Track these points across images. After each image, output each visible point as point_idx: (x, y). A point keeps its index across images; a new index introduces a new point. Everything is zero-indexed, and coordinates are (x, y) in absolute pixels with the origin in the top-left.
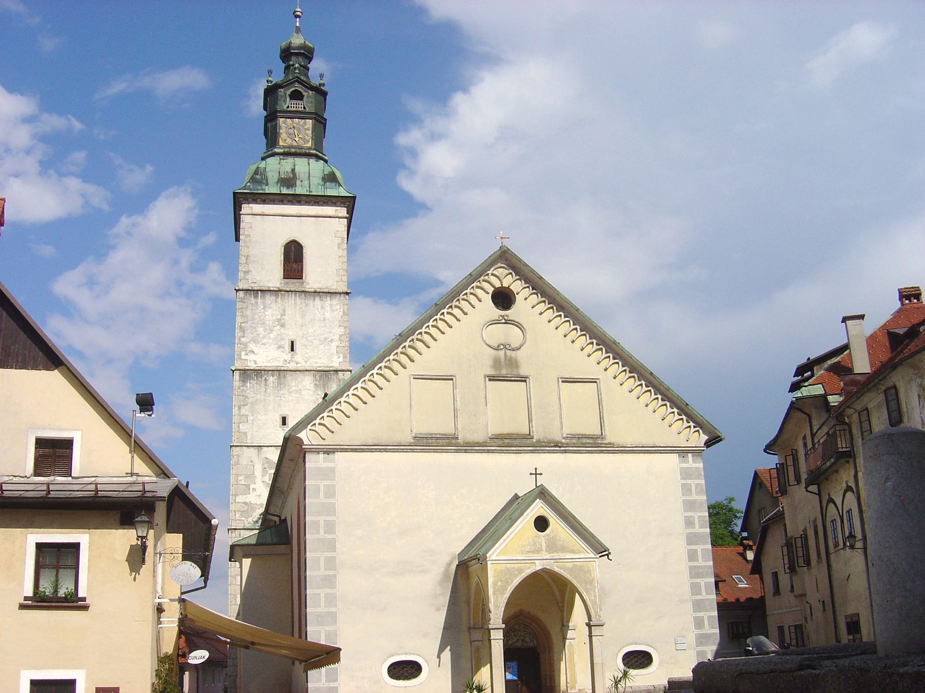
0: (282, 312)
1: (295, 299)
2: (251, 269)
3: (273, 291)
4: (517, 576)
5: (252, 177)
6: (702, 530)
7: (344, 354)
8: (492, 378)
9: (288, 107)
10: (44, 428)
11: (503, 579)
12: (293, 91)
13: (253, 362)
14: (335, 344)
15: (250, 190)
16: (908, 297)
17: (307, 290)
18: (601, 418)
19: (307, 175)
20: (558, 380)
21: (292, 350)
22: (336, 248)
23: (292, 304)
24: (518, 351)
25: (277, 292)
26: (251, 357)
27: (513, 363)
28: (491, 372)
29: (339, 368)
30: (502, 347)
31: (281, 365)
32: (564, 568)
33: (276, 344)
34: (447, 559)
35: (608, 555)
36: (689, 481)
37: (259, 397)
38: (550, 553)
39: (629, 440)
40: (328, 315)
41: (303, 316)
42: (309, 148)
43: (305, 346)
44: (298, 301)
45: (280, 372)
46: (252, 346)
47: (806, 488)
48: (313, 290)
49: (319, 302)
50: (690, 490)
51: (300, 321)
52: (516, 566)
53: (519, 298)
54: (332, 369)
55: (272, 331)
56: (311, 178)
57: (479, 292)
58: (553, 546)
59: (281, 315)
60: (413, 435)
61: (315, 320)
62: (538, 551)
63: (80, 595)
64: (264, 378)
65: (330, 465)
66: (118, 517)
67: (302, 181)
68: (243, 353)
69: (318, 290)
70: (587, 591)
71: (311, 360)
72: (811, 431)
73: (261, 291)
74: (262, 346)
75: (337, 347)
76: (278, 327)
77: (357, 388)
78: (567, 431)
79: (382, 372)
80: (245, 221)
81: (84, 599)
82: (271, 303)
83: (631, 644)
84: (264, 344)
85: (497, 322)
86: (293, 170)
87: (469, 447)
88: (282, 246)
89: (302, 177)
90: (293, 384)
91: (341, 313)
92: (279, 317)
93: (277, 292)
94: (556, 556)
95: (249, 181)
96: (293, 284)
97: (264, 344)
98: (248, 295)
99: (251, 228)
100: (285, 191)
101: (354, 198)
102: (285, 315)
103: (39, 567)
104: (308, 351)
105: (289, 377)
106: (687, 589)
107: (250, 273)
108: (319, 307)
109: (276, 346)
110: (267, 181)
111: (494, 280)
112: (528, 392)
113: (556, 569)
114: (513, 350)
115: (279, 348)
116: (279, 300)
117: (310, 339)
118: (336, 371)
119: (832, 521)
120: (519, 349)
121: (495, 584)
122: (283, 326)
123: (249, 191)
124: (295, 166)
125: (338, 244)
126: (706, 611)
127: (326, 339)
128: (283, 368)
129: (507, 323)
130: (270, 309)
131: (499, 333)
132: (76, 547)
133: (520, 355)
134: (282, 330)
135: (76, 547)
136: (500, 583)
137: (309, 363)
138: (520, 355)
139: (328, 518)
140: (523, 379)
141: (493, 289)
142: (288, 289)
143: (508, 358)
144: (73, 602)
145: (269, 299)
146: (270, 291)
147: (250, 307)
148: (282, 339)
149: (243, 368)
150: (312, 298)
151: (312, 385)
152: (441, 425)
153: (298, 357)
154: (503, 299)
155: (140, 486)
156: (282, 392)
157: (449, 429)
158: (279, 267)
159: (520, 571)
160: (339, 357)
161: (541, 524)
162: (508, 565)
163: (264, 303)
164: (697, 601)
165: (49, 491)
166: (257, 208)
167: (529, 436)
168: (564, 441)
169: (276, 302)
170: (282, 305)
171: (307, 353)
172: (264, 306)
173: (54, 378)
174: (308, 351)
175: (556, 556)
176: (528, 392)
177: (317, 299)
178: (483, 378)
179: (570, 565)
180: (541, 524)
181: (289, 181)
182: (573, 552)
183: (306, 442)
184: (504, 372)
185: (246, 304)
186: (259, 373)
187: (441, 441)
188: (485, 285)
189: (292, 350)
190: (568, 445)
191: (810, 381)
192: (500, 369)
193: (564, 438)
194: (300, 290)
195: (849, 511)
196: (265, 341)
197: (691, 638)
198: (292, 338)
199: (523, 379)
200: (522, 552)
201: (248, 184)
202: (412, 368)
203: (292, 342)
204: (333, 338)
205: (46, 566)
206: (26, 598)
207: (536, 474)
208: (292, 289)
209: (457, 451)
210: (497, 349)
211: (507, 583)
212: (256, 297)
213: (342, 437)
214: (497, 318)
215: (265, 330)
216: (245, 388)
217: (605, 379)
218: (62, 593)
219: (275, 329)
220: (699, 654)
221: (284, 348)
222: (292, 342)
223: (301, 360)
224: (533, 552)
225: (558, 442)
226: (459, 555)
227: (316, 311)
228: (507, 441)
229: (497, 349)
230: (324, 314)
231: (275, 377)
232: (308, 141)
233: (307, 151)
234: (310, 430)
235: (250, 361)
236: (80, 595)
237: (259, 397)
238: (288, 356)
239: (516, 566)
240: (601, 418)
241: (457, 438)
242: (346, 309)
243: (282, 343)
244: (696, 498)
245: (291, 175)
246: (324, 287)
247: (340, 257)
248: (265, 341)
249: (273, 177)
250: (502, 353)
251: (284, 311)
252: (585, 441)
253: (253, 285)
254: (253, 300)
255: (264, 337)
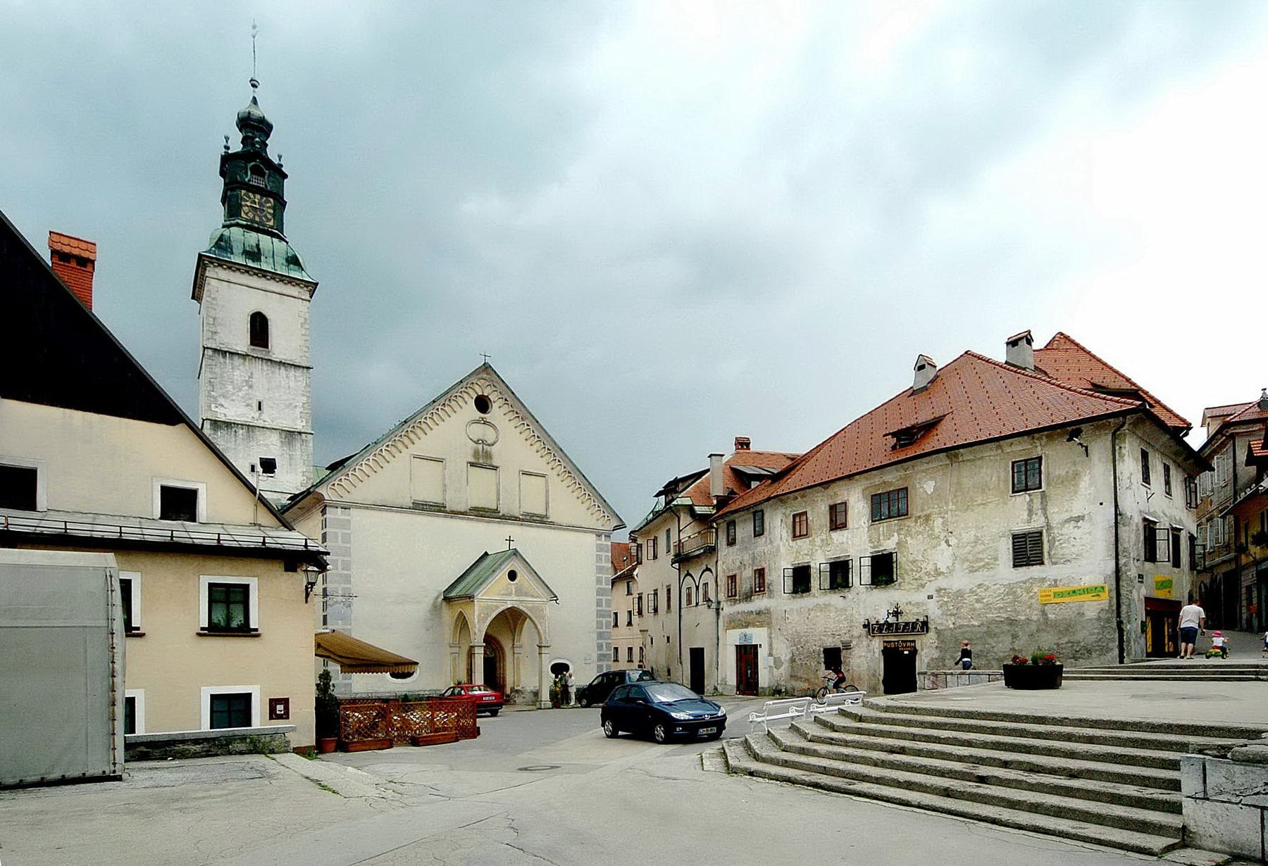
0: (249, 374)
1: (262, 365)
2: (219, 331)
3: (241, 354)
4: (494, 611)
5: (217, 242)
6: (607, 587)
7: (306, 419)
8: (472, 465)
9: (249, 180)
10: (168, 478)
11: (485, 612)
12: (253, 165)
13: (223, 415)
14: (298, 410)
15: (215, 254)
16: (742, 444)
17: (273, 359)
18: (547, 503)
19: (272, 253)
20: (519, 471)
21: (260, 409)
22: (299, 326)
23: (259, 370)
24: (493, 447)
25: (244, 356)
26: (220, 410)
27: (488, 455)
28: (472, 460)
29: (303, 431)
30: (480, 442)
31: (250, 420)
32: (527, 608)
33: (244, 402)
34: (436, 594)
35: (556, 600)
36: (601, 553)
37: (229, 445)
38: (517, 596)
39: (565, 521)
40: (292, 384)
41: (269, 382)
42: (272, 227)
43: (272, 407)
44: (265, 368)
45: (250, 428)
46: (221, 401)
47: (672, 565)
48: (278, 360)
49: (284, 372)
50: (601, 559)
51: (266, 386)
52: (495, 604)
53: (495, 406)
54: (296, 430)
55: (240, 390)
56: (275, 257)
57: (465, 396)
58: (519, 592)
59: (249, 377)
60: (413, 501)
61: (280, 386)
62: (510, 594)
63: (252, 626)
64: (233, 430)
65: (347, 518)
66: (282, 566)
67: (266, 258)
68: (213, 405)
69: (283, 361)
70: (541, 623)
71: (277, 421)
72: (679, 528)
73: (230, 353)
74: (232, 402)
75: (301, 412)
76: (247, 388)
77: (369, 459)
78: (523, 510)
79: (389, 449)
80: (211, 285)
81: (256, 630)
82: (240, 365)
83: (555, 659)
84: (233, 400)
85: (477, 422)
86: (258, 246)
87: (455, 514)
88: (248, 315)
89: (266, 254)
90: (261, 439)
91: (304, 384)
92: (247, 379)
93: (244, 356)
94: (522, 598)
95: (214, 246)
96: (259, 351)
97: (233, 400)
98: (216, 355)
99: (218, 291)
100: (250, 264)
101: (317, 284)
102: (252, 378)
103: (212, 601)
104: (274, 412)
105: (257, 432)
106: (594, 624)
107: (218, 335)
108: (285, 376)
109: (245, 404)
110: (232, 250)
111: (477, 388)
112: (547, 486)
113: (521, 608)
114: (489, 445)
115: (248, 405)
116: (247, 363)
117: (276, 402)
118: (300, 433)
119: (688, 588)
120: (493, 445)
121: (479, 615)
122: (251, 387)
123: (214, 256)
124: (259, 241)
125: (301, 323)
126: (605, 639)
127: (291, 404)
128: (251, 424)
129: (484, 423)
130: (238, 371)
131: (478, 431)
132: (245, 588)
133: (494, 450)
134: (250, 391)
135: (245, 588)
136: (482, 615)
137: (275, 423)
138: (494, 450)
139: (346, 559)
140: (495, 468)
141: (476, 395)
142: (255, 355)
143: (485, 451)
144: (245, 631)
145: (237, 361)
146: (238, 354)
147: (218, 365)
148: (250, 399)
149: (214, 418)
150: (278, 367)
151: (279, 442)
152: (433, 496)
153: (264, 416)
154: (482, 404)
155: (1068, 672)
156: (250, 444)
157: (438, 499)
158: (246, 334)
159: (497, 607)
160: (302, 421)
161: (512, 576)
162: (489, 603)
163: (232, 364)
164: (600, 632)
165: (264, 543)
166: (223, 274)
167: (496, 511)
168: (521, 517)
169: (244, 364)
170: (250, 368)
171: (273, 414)
172: (232, 367)
173: (181, 429)
174: (274, 412)
175: (522, 598)
176: (547, 486)
177: (283, 368)
178: (466, 464)
179: (530, 605)
180: (512, 576)
181: (255, 254)
182: (533, 596)
183: (326, 497)
184: (481, 461)
185: (214, 362)
186: (228, 425)
187: (433, 508)
188: (470, 391)
189: (260, 409)
190: (523, 520)
191: (682, 494)
192: (478, 459)
193: (522, 515)
194: (266, 358)
195: (706, 584)
196: (234, 397)
197: (595, 656)
198: (260, 399)
199: (495, 468)
200: (498, 594)
201: (213, 249)
202: (414, 450)
203: (260, 403)
204: (297, 404)
205: (217, 602)
206: (203, 629)
207: (510, 540)
208: (259, 356)
209: (445, 517)
210: (477, 443)
211: (488, 615)
212: (224, 357)
213: (356, 496)
214: (477, 418)
215: (234, 389)
216: (215, 436)
217: (552, 475)
218: (234, 624)
219: (244, 388)
220: (600, 667)
221: (252, 407)
222: (260, 403)
223: (267, 418)
224: (506, 595)
225: (517, 518)
226: (444, 592)
227: (281, 379)
228: (481, 513)
229: (477, 443)
230: (289, 383)
231: (244, 430)
232: (271, 220)
233: (270, 229)
234: (330, 488)
235: (220, 413)
236: (252, 626)
237: (229, 445)
238: (257, 415)
239: (495, 604)
240: (547, 503)
241: (445, 507)
242: (308, 382)
243: (250, 402)
244: (604, 565)
245: (256, 250)
246: (289, 359)
247: (302, 335)
248: (234, 397)
249: (238, 249)
250: (480, 446)
251: (252, 374)
252: (535, 518)
253: (221, 346)
254: (221, 360)
255: (233, 394)
